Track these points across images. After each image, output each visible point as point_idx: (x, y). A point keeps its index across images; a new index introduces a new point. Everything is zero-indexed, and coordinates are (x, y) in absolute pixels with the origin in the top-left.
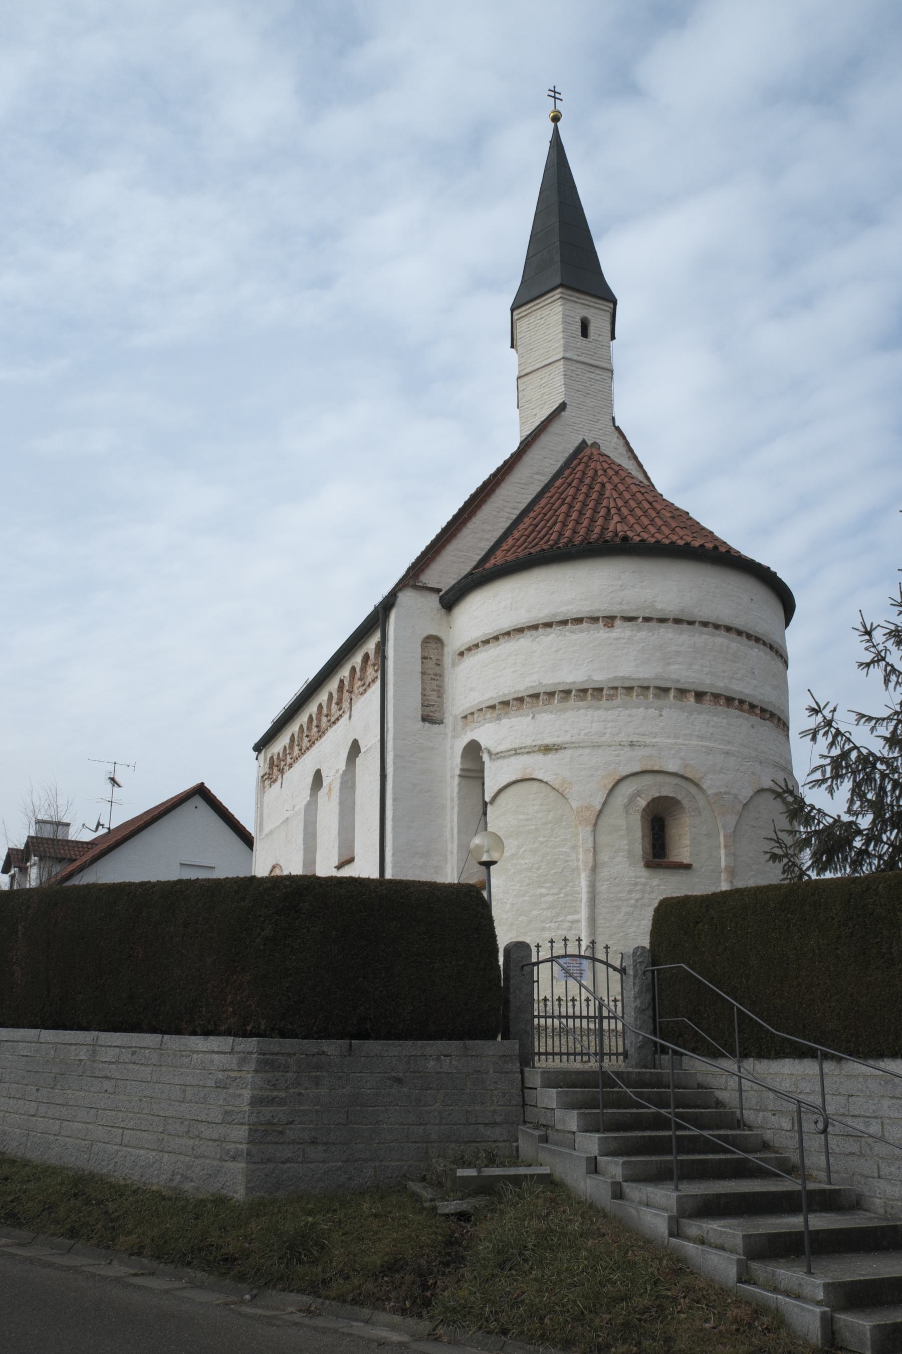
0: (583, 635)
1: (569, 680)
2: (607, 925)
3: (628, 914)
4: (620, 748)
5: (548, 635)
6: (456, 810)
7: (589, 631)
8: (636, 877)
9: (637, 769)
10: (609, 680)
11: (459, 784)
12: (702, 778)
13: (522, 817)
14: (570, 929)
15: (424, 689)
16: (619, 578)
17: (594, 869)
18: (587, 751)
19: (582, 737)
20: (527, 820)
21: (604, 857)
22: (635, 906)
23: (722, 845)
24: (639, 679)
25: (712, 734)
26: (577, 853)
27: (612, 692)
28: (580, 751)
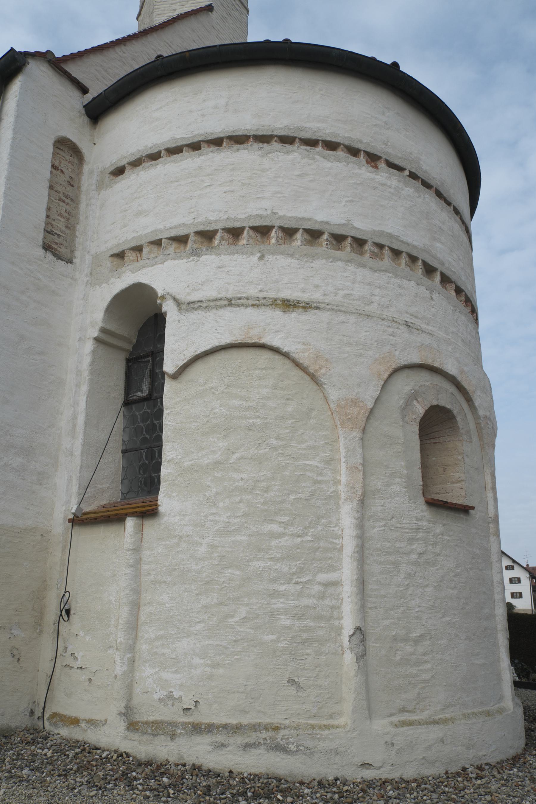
2: (383, 592)
3: (409, 576)
6: (84, 388)
7: (348, 163)
9: (416, 359)
11: (94, 352)
14: (322, 597)
15: (49, 209)
16: (383, 114)
18: (353, 319)
19: (339, 298)
20: (248, 409)
22: (416, 564)
24: (408, 244)
27: (376, 250)
28: (342, 317)
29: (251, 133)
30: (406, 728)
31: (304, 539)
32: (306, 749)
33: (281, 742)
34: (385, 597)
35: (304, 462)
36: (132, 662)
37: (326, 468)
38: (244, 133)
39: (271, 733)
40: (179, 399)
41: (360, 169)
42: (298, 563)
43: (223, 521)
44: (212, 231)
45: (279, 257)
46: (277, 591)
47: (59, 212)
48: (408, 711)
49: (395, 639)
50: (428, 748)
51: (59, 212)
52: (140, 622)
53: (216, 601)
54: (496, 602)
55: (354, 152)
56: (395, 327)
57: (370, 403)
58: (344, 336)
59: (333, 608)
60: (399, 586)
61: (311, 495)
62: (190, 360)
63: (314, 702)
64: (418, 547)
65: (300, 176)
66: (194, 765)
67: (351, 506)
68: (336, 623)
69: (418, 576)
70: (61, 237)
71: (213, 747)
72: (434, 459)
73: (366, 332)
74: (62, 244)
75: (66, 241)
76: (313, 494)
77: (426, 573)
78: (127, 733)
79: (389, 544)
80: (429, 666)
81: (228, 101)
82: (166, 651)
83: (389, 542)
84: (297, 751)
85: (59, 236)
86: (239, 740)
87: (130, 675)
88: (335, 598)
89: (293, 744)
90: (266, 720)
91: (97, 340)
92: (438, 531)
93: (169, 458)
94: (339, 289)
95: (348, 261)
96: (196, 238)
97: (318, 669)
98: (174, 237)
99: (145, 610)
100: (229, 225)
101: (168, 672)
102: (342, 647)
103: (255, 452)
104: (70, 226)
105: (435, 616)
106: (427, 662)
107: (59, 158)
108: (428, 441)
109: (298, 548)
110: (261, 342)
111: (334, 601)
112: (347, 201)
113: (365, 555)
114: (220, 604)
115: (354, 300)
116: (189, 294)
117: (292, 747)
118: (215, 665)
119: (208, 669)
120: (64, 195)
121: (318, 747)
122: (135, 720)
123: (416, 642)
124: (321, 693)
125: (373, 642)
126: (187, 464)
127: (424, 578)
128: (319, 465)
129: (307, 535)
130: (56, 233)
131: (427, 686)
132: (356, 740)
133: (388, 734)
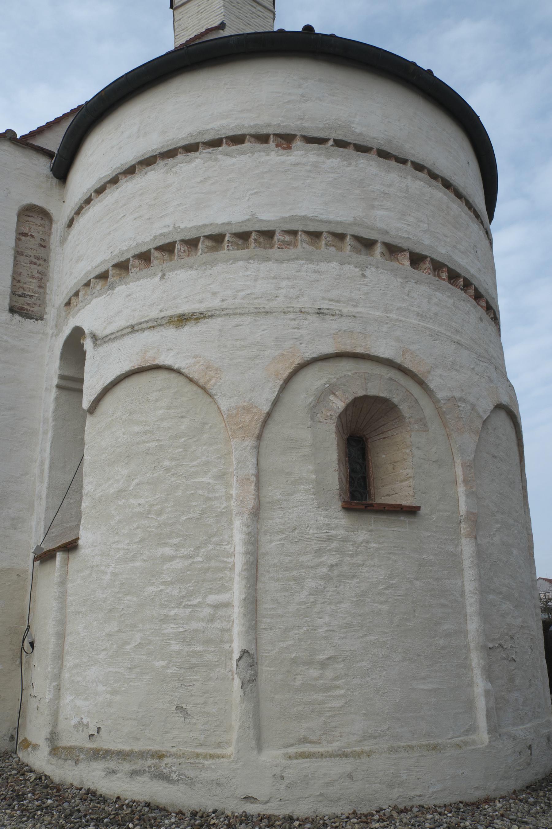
0: (244, 157)
1: (220, 221)
2: (280, 611)
3: (315, 592)
4: (301, 316)
5: (190, 162)
6: (50, 435)
8: (329, 527)
9: (329, 348)
10: (284, 220)
11: (56, 399)
12: (429, 372)
13: (136, 429)
14: (212, 619)
17: (256, 513)
18: (248, 319)
19: (238, 300)
21: (273, 492)
22: (327, 578)
23: (460, 479)
24: (330, 222)
25: (436, 314)
26: (228, 486)
27: (287, 238)
28: (236, 320)
29: (157, 153)
30: (300, 761)
31: (195, 560)
32: (187, 779)
33: (164, 771)
34: (283, 616)
35: (196, 480)
36: (58, 690)
37: (219, 484)
38: (151, 155)
39: (155, 761)
40: (94, 433)
41: (268, 155)
42: (188, 585)
43: (124, 549)
44: (125, 261)
45: (178, 272)
46: (168, 616)
47: (30, 274)
48: (311, 742)
49: (294, 662)
50: (329, 784)
51: (30, 274)
52: (65, 652)
53: (116, 629)
54: (468, 616)
55: (263, 139)
56: (301, 318)
57: (265, 407)
58: (237, 340)
59: (223, 630)
60: (302, 603)
61: (202, 514)
62: (100, 393)
63: (201, 730)
64: (330, 559)
65: (201, 182)
66: (89, 789)
67: (240, 521)
68: (227, 646)
69: (329, 591)
70: (34, 297)
71: (106, 773)
72: (384, 456)
73: (263, 330)
74: (35, 304)
75: (40, 300)
76: (203, 512)
77: (341, 587)
78: (49, 757)
79: (289, 558)
80: (342, 692)
81: (140, 127)
82: (80, 679)
83: (290, 556)
84: (178, 780)
85: (31, 296)
86: (127, 767)
87: (56, 702)
88: (225, 621)
89: (175, 773)
90: (155, 747)
91: (58, 386)
92: (360, 539)
93: (86, 491)
94: (238, 291)
95: (250, 258)
96: (114, 271)
97: (206, 695)
98: (99, 275)
99: (69, 639)
100: (138, 252)
101: (80, 699)
102: (231, 671)
103: (151, 476)
104: (43, 285)
105: (353, 635)
106: (338, 687)
107: (29, 224)
108: (378, 437)
109: (188, 570)
110: (155, 363)
111: (224, 624)
112: (251, 195)
113: (259, 572)
114: (120, 631)
115: (255, 299)
116: (105, 328)
117: (174, 776)
118: (114, 692)
119: (108, 696)
120: (35, 257)
121: (200, 777)
122: (58, 745)
123: (324, 665)
124: (209, 721)
125: (266, 666)
126: (98, 495)
127: (338, 593)
128: (211, 481)
129: (198, 556)
130: (28, 295)
131: (339, 714)
132: (433, 781)
133: (277, 766)
